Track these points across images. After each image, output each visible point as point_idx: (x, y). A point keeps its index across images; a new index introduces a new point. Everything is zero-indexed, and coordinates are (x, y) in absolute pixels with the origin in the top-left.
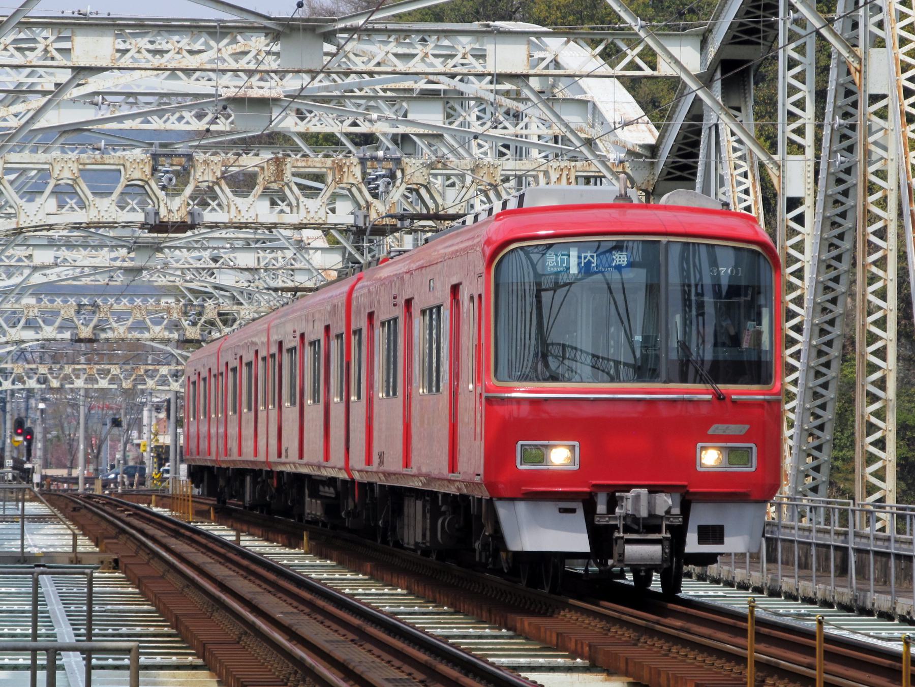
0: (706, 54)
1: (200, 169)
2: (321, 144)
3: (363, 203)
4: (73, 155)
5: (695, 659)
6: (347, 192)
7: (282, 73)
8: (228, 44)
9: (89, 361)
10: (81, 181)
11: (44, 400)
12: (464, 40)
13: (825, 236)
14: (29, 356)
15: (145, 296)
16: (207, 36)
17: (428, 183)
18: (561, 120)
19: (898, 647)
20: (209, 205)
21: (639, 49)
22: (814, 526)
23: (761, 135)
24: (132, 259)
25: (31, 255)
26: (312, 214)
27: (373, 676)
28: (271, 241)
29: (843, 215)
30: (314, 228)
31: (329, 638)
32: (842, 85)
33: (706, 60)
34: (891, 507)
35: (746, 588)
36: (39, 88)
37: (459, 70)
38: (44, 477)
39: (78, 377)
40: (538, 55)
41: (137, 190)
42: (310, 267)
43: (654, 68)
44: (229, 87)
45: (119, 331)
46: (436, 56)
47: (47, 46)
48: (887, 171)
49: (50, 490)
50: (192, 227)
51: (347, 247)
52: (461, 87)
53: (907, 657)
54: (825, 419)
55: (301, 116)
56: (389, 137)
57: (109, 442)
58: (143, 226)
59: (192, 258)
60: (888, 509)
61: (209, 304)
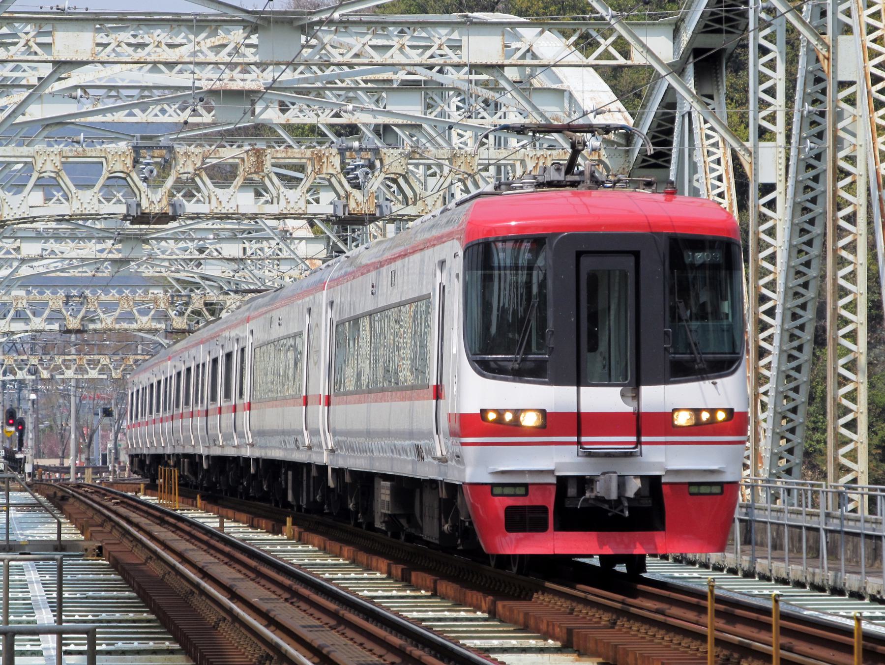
0: (679, 43)
1: (181, 160)
2: (308, 135)
3: (342, 193)
4: (56, 148)
5: (663, 638)
6: (327, 183)
7: (262, 66)
8: (207, 38)
9: (79, 352)
10: (63, 174)
11: (35, 391)
12: (443, 31)
13: (796, 221)
14: (19, 346)
15: (133, 287)
16: (187, 31)
17: (407, 173)
18: (534, 108)
19: (852, 623)
20: (195, 196)
21: (611, 39)
22: (787, 508)
23: (742, 122)
24: (119, 251)
25: (19, 248)
26: (292, 204)
27: (336, 656)
28: (257, 231)
29: (814, 200)
30: (295, 218)
31: (304, 623)
32: (811, 72)
33: (679, 48)
34: (863, 488)
35: (721, 570)
36: (24, 82)
37: (438, 60)
38: (36, 468)
39: (68, 368)
40: (514, 45)
41: (118, 182)
42: (293, 256)
43: (626, 55)
44: (207, 80)
45: (107, 321)
46: (411, 47)
47: (28, 41)
48: (856, 157)
49: (42, 480)
50: (174, 218)
51: (331, 236)
52: (439, 78)
53: (858, 634)
54: (798, 402)
55: (284, 108)
56: (372, 128)
57: (101, 432)
58: (125, 218)
59: (179, 249)
60: (860, 490)
61: (196, 295)
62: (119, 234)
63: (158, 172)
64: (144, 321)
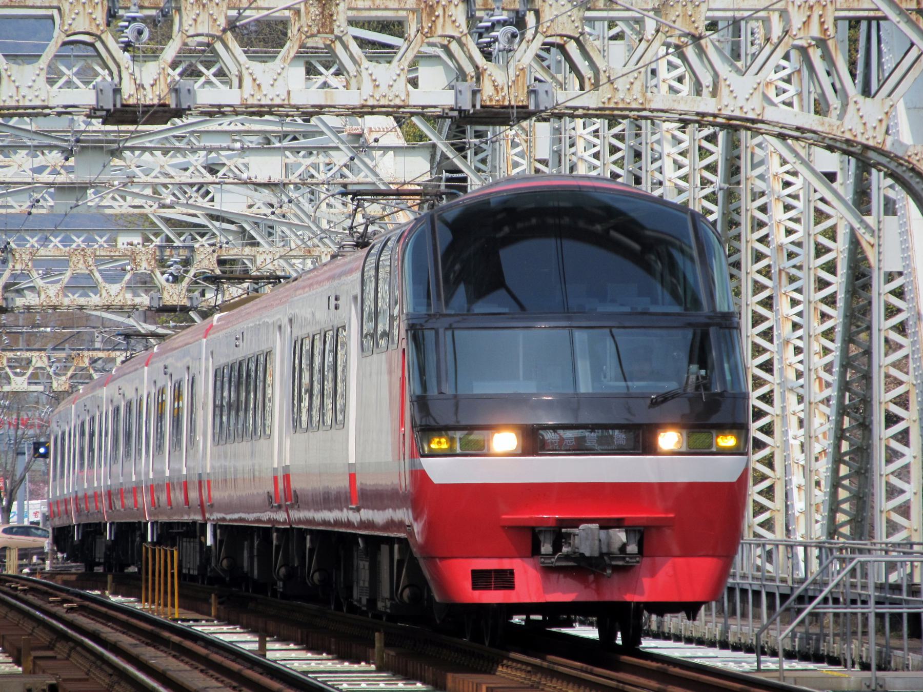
24: (70, 170)
26: (383, 89)
28: (306, 135)
50: (179, 113)
58: (93, 113)
62: (78, 141)
63: (150, 31)
64: (115, 293)
